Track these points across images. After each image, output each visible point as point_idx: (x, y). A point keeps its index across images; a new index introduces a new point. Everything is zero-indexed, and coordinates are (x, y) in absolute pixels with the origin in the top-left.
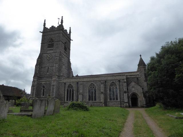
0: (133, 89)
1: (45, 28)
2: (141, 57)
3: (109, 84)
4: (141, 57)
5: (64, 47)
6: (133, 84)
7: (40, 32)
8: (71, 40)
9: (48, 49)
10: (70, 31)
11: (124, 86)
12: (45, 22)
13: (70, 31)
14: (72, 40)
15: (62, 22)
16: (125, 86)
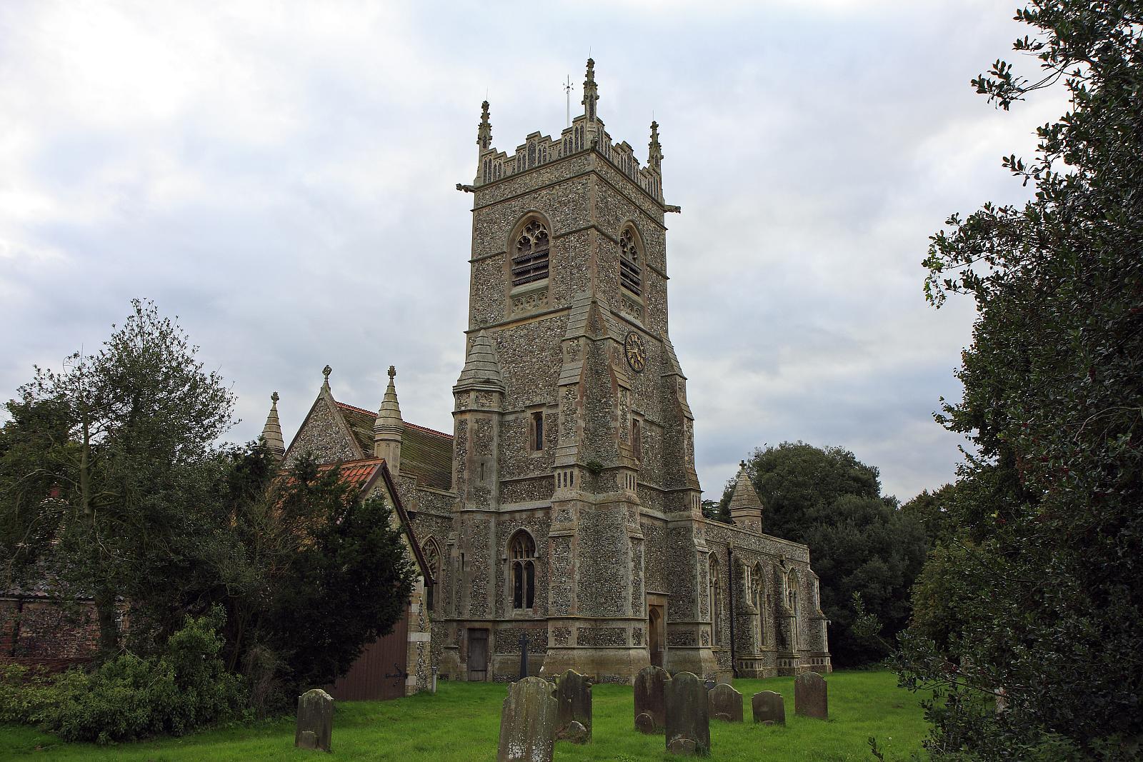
1: (488, 158)
7: (459, 187)
10: (655, 146)
13: (655, 146)
14: (677, 209)
15: (590, 98)
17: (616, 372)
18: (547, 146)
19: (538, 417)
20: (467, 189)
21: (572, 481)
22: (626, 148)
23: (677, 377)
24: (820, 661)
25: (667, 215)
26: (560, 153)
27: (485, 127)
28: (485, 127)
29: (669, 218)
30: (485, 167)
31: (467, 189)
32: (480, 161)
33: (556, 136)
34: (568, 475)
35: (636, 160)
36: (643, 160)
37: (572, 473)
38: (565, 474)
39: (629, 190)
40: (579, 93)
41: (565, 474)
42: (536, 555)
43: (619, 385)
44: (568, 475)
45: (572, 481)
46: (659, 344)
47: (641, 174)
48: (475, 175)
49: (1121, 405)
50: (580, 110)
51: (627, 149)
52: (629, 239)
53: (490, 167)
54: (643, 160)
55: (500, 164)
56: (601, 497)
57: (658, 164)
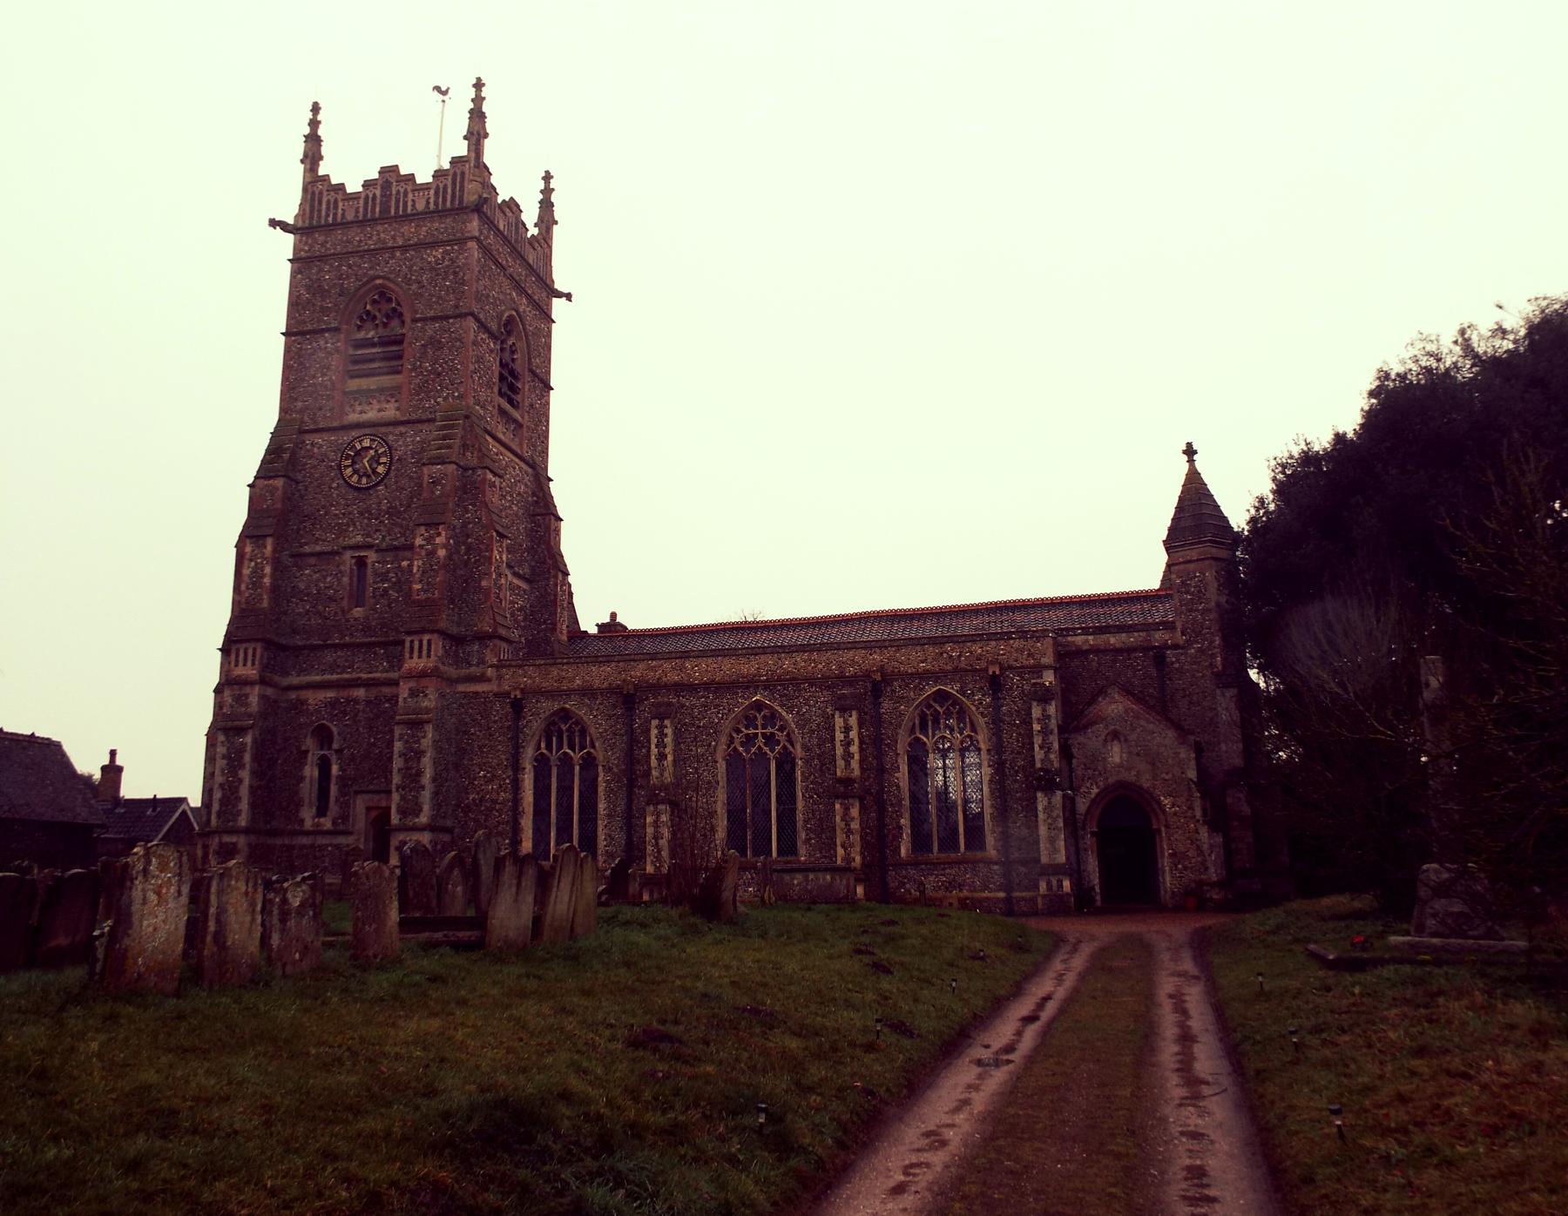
0: (1116, 754)
1: (317, 189)
2: (1191, 461)
3: (909, 712)
4: (1191, 461)
5: (496, 368)
6: (1114, 706)
7: (274, 223)
8: (559, 295)
9: (354, 384)
10: (546, 206)
11: (1037, 727)
12: (314, 124)
13: (546, 206)
14: (569, 297)
15: (477, 133)
16: (1045, 732)
17: (494, 515)
18: (409, 188)
19: (361, 563)
20: (284, 226)
21: (429, 650)
22: (512, 206)
25: (555, 300)
27: (313, 141)
28: (313, 141)
29: (558, 305)
31: (284, 226)
32: (305, 190)
34: (425, 643)
35: (524, 225)
36: (530, 216)
37: (429, 642)
38: (421, 642)
39: (518, 270)
40: (462, 124)
42: (335, 746)
44: (425, 643)
46: (530, 470)
47: (530, 244)
48: (296, 210)
49: (327, 845)
50: (462, 149)
51: (515, 208)
53: (320, 203)
54: (530, 216)
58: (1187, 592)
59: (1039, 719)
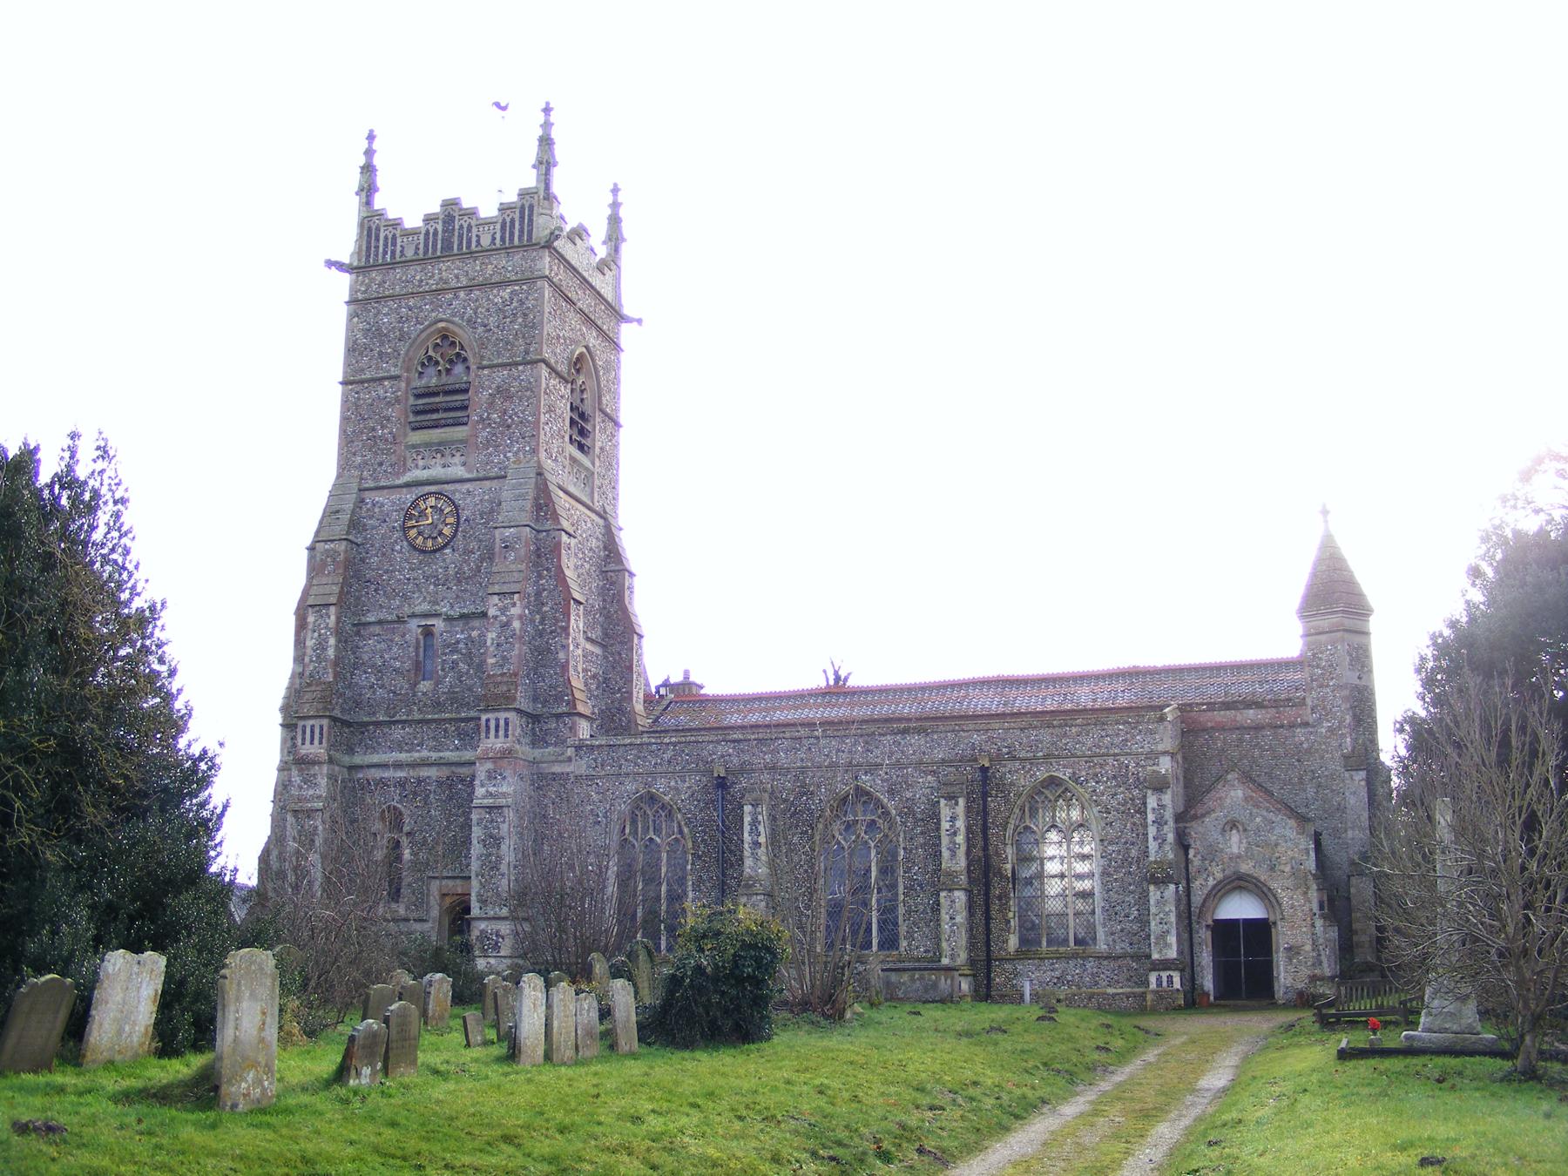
7: (330, 264)
10: (615, 221)
13: (615, 221)
15: (545, 164)
20: (340, 266)
23: (563, 533)
24: (1165, 984)
26: (494, 238)
29: (626, 333)
30: (369, 236)
31: (340, 266)
33: (488, 210)
41: (497, 720)
43: (574, 599)
44: (502, 723)
45: (506, 730)
46: (601, 522)
50: (530, 180)
52: (578, 371)
55: (394, 236)
56: (537, 753)
57: (617, 250)
58: (1318, 667)
59: (1154, 809)
